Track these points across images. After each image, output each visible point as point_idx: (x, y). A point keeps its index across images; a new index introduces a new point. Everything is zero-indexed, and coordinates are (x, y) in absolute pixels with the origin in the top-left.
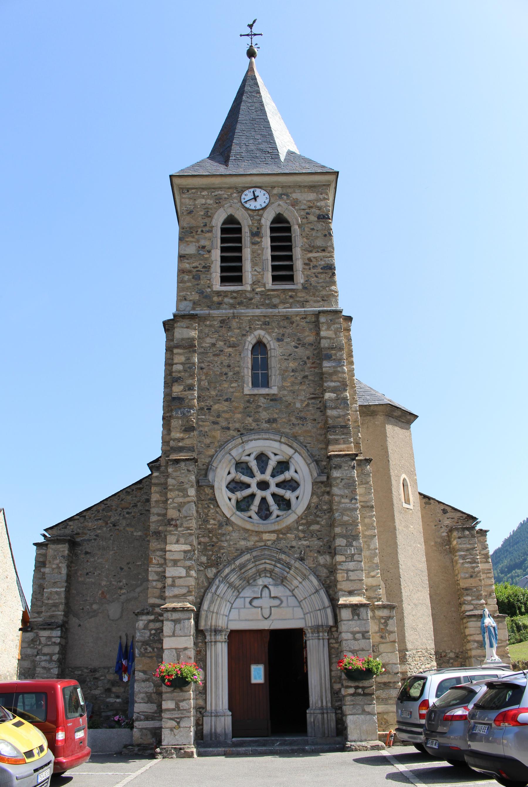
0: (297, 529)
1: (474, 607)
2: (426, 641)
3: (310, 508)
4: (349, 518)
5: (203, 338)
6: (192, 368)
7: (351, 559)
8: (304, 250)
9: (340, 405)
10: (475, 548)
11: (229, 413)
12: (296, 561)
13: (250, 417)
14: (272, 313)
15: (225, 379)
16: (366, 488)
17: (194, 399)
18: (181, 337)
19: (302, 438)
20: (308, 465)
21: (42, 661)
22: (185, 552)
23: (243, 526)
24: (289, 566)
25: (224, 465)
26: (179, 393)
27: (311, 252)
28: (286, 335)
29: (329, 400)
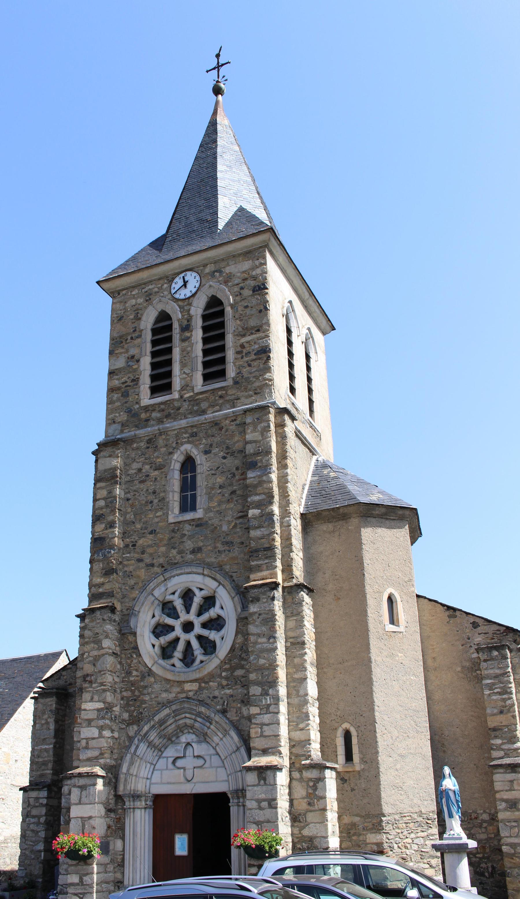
0: (220, 676)
1: (505, 754)
2: (419, 802)
3: (234, 650)
4: (265, 661)
5: (130, 464)
6: (113, 502)
7: (267, 711)
8: (237, 335)
9: (264, 523)
10: (506, 673)
11: (153, 547)
12: (215, 714)
13: (174, 548)
14: (198, 421)
15: (150, 508)
16: (296, 620)
17: (114, 537)
18: (103, 469)
19: (228, 567)
20: (233, 598)
21: (31, 824)
22: (98, 710)
23: (164, 676)
24: (209, 720)
25: (147, 608)
26: (101, 533)
27: (244, 336)
28: (214, 445)
29: (252, 518)
